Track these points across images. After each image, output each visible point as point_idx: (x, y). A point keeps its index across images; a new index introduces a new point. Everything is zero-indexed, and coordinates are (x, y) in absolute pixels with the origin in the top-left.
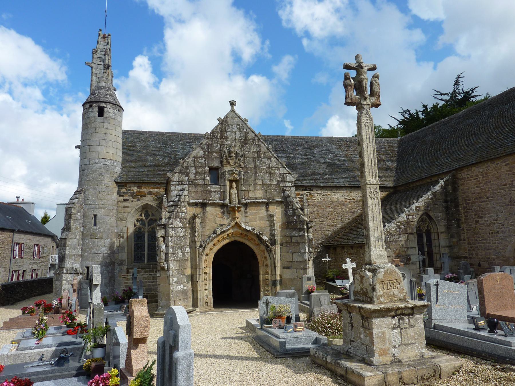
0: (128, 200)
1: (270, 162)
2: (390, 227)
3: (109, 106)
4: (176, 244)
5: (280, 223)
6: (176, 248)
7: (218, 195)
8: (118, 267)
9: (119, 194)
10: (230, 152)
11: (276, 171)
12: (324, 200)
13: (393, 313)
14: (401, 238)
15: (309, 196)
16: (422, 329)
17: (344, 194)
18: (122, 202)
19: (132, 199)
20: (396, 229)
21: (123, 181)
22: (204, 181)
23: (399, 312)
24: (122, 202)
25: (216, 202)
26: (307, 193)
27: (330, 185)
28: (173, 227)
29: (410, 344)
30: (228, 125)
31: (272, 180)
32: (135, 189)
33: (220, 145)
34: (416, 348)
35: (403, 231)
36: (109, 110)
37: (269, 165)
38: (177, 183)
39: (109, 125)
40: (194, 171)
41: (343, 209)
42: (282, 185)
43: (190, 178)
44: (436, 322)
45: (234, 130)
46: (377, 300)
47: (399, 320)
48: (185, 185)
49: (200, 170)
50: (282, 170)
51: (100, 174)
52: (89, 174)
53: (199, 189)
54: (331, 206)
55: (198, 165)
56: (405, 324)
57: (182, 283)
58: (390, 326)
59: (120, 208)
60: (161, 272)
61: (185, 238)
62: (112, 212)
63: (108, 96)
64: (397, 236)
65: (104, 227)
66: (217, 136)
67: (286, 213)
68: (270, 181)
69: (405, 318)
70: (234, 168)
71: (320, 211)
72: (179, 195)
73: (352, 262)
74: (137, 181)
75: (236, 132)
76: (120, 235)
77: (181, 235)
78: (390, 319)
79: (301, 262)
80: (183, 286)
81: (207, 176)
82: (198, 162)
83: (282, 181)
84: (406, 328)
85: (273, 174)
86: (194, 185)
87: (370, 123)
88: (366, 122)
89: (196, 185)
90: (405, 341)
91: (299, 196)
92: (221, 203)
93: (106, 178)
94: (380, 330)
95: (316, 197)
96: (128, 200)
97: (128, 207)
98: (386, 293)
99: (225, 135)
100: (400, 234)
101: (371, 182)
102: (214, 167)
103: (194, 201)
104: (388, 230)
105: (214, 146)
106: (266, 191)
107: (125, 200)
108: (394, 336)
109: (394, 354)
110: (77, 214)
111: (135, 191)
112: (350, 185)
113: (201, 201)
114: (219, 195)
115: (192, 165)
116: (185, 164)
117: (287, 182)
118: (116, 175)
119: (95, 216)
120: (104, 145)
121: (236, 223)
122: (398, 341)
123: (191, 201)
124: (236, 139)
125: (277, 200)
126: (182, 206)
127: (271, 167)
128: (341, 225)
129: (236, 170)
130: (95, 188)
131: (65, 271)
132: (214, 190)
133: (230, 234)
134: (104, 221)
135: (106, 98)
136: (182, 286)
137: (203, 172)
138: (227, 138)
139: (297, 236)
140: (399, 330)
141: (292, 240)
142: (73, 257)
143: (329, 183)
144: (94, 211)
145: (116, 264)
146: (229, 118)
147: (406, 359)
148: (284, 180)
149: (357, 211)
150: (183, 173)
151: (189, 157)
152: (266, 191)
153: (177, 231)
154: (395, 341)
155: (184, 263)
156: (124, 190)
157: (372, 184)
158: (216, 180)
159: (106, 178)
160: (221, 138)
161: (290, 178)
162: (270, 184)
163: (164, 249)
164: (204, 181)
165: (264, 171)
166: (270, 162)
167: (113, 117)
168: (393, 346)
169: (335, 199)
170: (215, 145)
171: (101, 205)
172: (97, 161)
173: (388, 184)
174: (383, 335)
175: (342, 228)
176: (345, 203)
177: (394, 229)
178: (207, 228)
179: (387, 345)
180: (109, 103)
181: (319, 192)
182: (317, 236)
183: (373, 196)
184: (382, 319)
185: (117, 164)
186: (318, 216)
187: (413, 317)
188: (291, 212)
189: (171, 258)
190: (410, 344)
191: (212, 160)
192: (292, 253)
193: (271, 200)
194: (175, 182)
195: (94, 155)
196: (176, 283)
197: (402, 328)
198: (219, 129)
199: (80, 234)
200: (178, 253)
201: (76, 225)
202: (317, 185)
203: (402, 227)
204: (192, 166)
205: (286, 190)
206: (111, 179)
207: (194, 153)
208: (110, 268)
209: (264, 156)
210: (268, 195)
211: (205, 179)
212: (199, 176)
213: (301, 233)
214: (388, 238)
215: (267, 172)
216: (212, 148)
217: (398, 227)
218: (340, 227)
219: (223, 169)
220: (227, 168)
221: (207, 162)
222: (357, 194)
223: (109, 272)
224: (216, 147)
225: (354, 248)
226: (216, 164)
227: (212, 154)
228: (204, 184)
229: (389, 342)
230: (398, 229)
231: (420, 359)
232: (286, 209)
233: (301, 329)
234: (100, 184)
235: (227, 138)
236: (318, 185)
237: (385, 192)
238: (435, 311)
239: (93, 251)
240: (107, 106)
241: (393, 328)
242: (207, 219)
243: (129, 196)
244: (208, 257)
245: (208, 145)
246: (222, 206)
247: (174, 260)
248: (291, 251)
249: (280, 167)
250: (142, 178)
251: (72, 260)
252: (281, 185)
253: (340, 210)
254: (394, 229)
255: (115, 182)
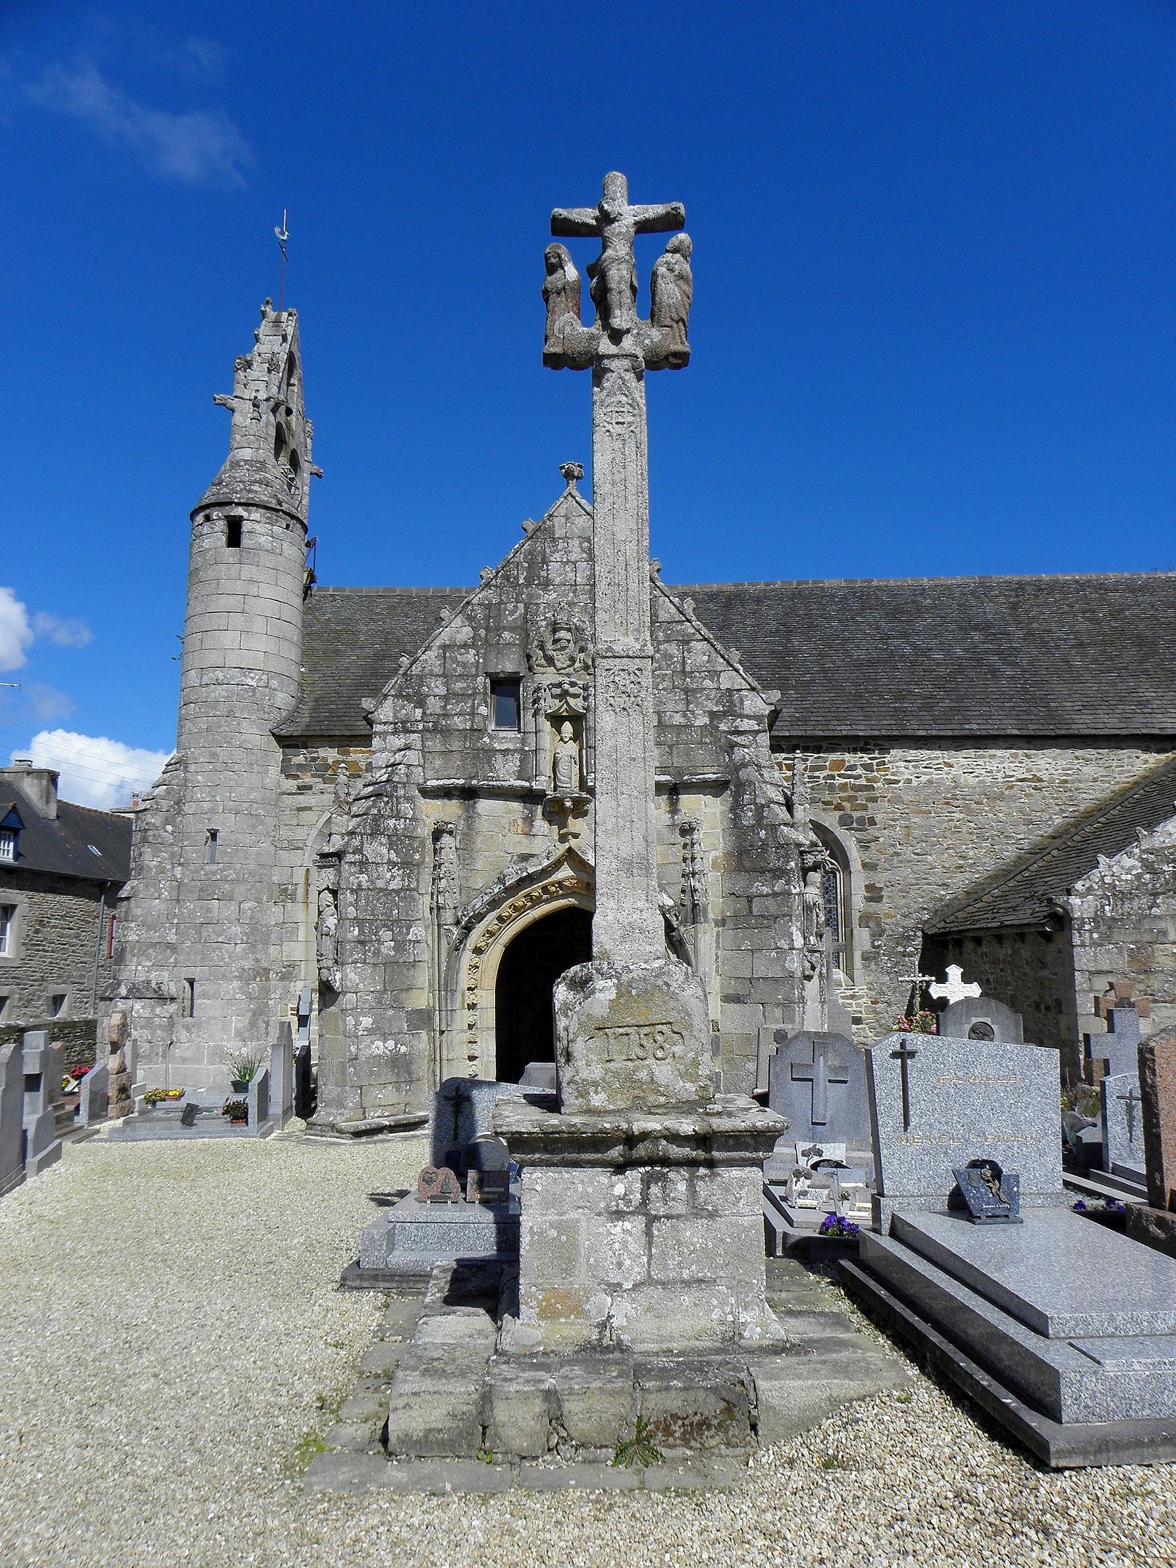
0: (310, 788)
1: (686, 654)
2: (1114, 869)
3: (256, 515)
4: (374, 916)
5: (719, 853)
6: (371, 925)
7: (514, 763)
8: (280, 984)
9: (287, 771)
10: (555, 627)
11: (708, 683)
12: (930, 782)
13: (616, 1153)
14: (1158, 907)
15: (878, 770)
16: (752, 1226)
17: (1003, 762)
18: (294, 794)
19: (322, 786)
20: (1139, 877)
21: (295, 734)
22: (470, 720)
23: (641, 1150)
24: (294, 794)
25: (506, 784)
26: (870, 759)
27: (950, 733)
28: (361, 862)
29: (687, 1284)
30: (554, 540)
31: (693, 712)
32: (330, 754)
33: (525, 605)
34: (715, 1302)
35: (1167, 883)
36: (257, 526)
37: (684, 664)
38: (390, 728)
39: (254, 569)
40: (442, 691)
41: (1001, 811)
42: (726, 729)
43: (428, 712)
44: (902, 1209)
45: (573, 557)
46: (577, 1098)
47: (647, 1182)
48: (414, 732)
49: (459, 685)
50: (728, 680)
51: (229, 712)
52: (199, 715)
53: (456, 745)
54: (956, 803)
55: (455, 670)
56: (673, 1199)
57: (390, 1034)
58: (602, 1205)
59: (287, 812)
60: (327, 997)
61: (405, 898)
62: (263, 823)
63: (256, 488)
64: (1145, 901)
65: (238, 866)
66: (517, 578)
67: (734, 819)
68: (685, 716)
69: (672, 1175)
70: (568, 675)
71: (916, 820)
72: (393, 765)
73: (966, 979)
74: (337, 733)
75: (577, 561)
76: (287, 889)
77: (391, 887)
78: (602, 1177)
79: (776, 980)
80: (396, 1044)
81: (479, 705)
82: (455, 660)
83: (724, 714)
84: (678, 1217)
85: (694, 691)
86: (441, 732)
87: (630, 424)
88: (614, 421)
89: (446, 733)
90: (665, 1267)
91: (843, 772)
92: (522, 787)
93: (245, 723)
94: (552, 1216)
95: (902, 773)
96: (310, 788)
97: (310, 809)
98: (616, 1074)
99: (544, 574)
100: (1156, 895)
101: (618, 648)
102: (502, 675)
103: (441, 782)
104: (1108, 880)
105: (506, 609)
106: (670, 747)
107: (303, 789)
108: (617, 1246)
109: (610, 1317)
110: (164, 827)
111: (330, 761)
112: (1025, 732)
113: (461, 781)
114: (518, 764)
115: (437, 670)
116: (416, 670)
117: (742, 716)
118: (276, 716)
119: (214, 835)
120: (240, 628)
121: (570, 850)
122: (637, 1272)
123: (432, 783)
124: (576, 585)
125: (706, 776)
126: (397, 798)
127: (688, 669)
128: (990, 865)
129: (573, 684)
130: (215, 754)
131: (123, 991)
132: (504, 747)
133: (553, 885)
134: (236, 851)
135: (250, 491)
136: (391, 1044)
137: (470, 692)
138: (546, 584)
139: (767, 895)
140: (636, 1225)
141: (751, 907)
142: (151, 951)
143: (949, 727)
144: (209, 819)
145: (272, 975)
146: (555, 520)
147: (653, 1341)
148: (732, 711)
149: (1051, 818)
150: (408, 698)
151: (428, 648)
152: (670, 747)
153: (375, 875)
154: (620, 1265)
155: (401, 972)
156: (300, 759)
157: (622, 653)
158: (510, 717)
159: (245, 723)
160: (529, 582)
161: (757, 704)
162: (686, 726)
163: (333, 928)
164: (470, 720)
165: (665, 684)
166: (686, 654)
167: (269, 547)
168: (609, 1285)
169: (971, 780)
170: (510, 606)
171: (231, 803)
172: (220, 675)
173: (1170, 725)
174: (564, 1238)
175: (993, 877)
176: (1007, 793)
177: (1129, 877)
178: (479, 866)
179: (581, 1278)
180: (258, 506)
181: (912, 754)
182: (903, 901)
183: (621, 701)
184: (567, 1174)
185: (281, 683)
186: (908, 835)
187: (714, 1175)
188: (750, 814)
189: (351, 955)
190: (687, 1284)
191: (499, 653)
192: (752, 950)
193: (686, 777)
194: (385, 723)
195: (213, 658)
196: (370, 1032)
197: (657, 1218)
198: (525, 556)
199: (171, 887)
200: (378, 940)
201: (159, 859)
202: (903, 733)
203: (1165, 868)
204: (437, 676)
205: (737, 744)
206: (259, 728)
207: (444, 636)
208: (254, 986)
209: (666, 635)
210: (678, 762)
211: (473, 714)
212: (458, 703)
213: (779, 885)
214: (1107, 908)
215: (674, 687)
216: (499, 616)
217: (1149, 867)
218: (986, 874)
219: (533, 682)
220: (547, 677)
221: (481, 660)
222: (1050, 761)
223: (250, 998)
224: (513, 613)
225: (1006, 943)
226: (509, 665)
227: (500, 636)
228: (472, 729)
229: (589, 1265)
230: (1148, 876)
231: (717, 1351)
232: (736, 808)
233: (493, 1193)
234: (229, 743)
235: (546, 584)
236: (910, 733)
237: (1158, 752)
238: (896, 1162)
239: (205, 934)
240: (250, 514)
241: (617, 1212)
242: (479, 839)
243: (313, 776)
244: (484, 957)
245: (489, 606)
246: (530, 797)
247: (364, 962)
248: (747, 945)
249: (720, 669)
250: (352, 723)
251: (148, 959)
252: (723, 727)
253: (987, 816)
254: (1129, 877)
255: (274, 735)
